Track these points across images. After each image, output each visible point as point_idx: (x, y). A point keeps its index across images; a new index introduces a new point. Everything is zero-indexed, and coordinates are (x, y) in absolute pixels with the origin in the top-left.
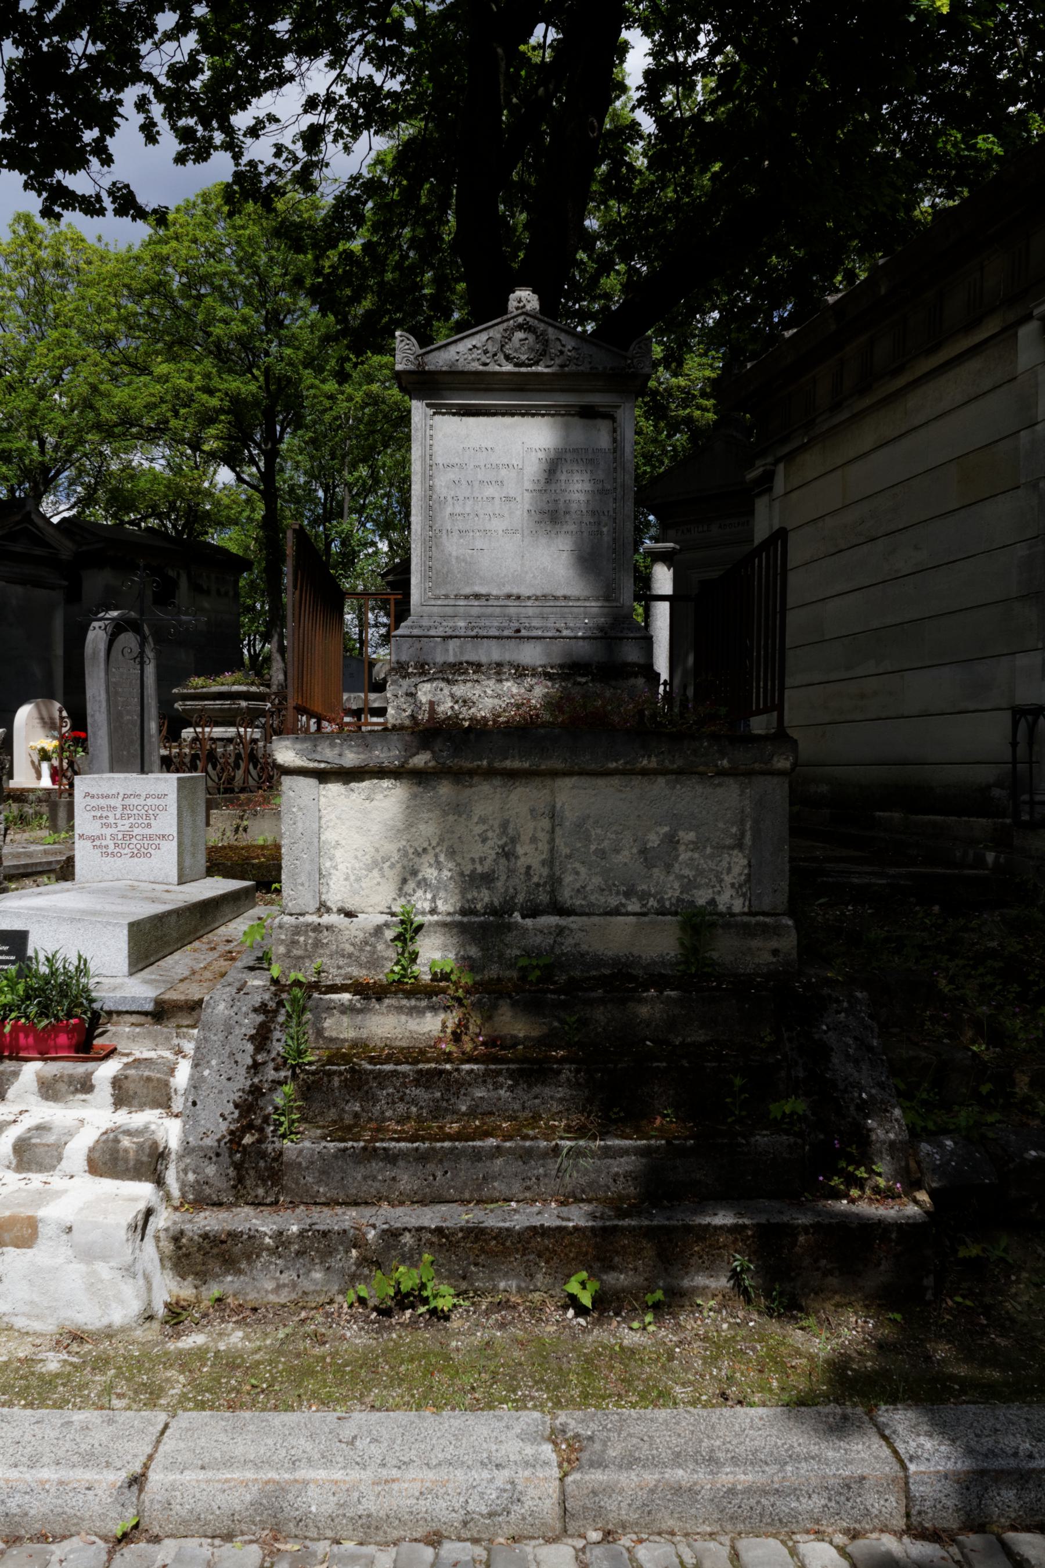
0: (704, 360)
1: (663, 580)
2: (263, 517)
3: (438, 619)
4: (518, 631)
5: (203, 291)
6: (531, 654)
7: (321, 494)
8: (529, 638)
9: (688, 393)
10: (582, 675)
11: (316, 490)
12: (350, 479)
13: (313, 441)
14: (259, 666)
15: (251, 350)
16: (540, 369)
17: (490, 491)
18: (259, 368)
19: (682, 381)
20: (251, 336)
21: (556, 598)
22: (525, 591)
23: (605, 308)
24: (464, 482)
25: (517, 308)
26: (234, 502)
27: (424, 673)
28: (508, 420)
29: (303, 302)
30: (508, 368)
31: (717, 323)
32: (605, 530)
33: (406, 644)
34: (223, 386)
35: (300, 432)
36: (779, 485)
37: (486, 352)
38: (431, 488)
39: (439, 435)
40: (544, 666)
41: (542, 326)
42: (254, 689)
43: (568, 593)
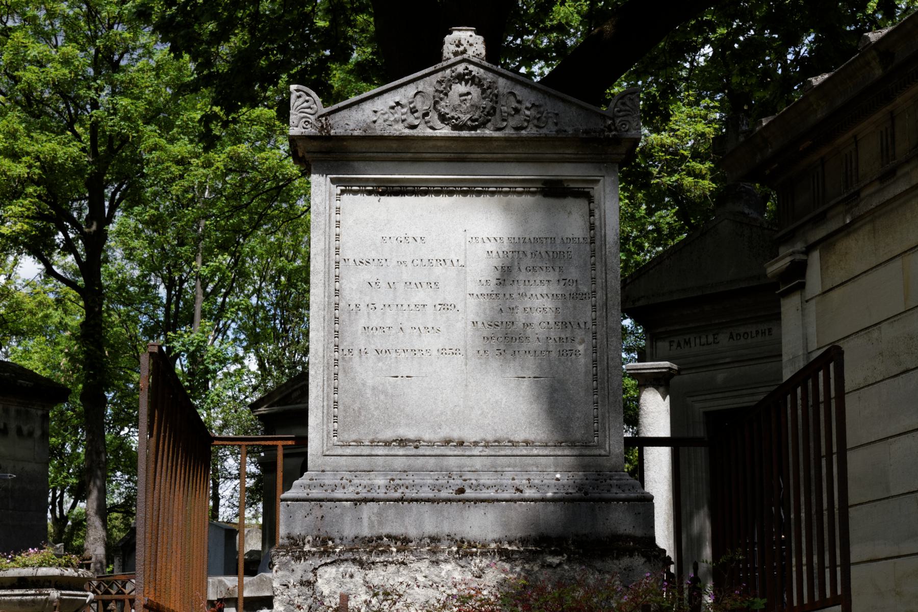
0: (695, 110)
1: (656, 415)
2: (83, 325)
3: (347, 475)
4: (461, 491)
5: (10, 24)
6: (481, 525)
7: (162, 292)
8: (476, 501)
9: (675, 153)
10: (554, 554)
11: (155, 287)
12: (204, 271)
13: (152, 222)
14: (69, 534)
15: (73, 100)
16: (488, 132)
17: (420, 296)
18: (82, 125)
19: (665, 138)
20: (74, 82)
21: (514, 444)
22: (470, 435)
23: (560, 46)
24: (383, 284)
25: (456, 54)
26: (40, 303)
27: (326, 553)
28: (443, 200)
29: (146, 37)
30: (445, 131)
31: (711, 61)
32: (581, 348)
33: (301, 510)
34: (34, 148)
35: (137, 209)
36: (814, 280)
37: (413, 111)
38: (337, 292)
39: (348, 220)
40: (499, 541)
41: (489, 77)
42: (70, 572)
43: (531, 437)
